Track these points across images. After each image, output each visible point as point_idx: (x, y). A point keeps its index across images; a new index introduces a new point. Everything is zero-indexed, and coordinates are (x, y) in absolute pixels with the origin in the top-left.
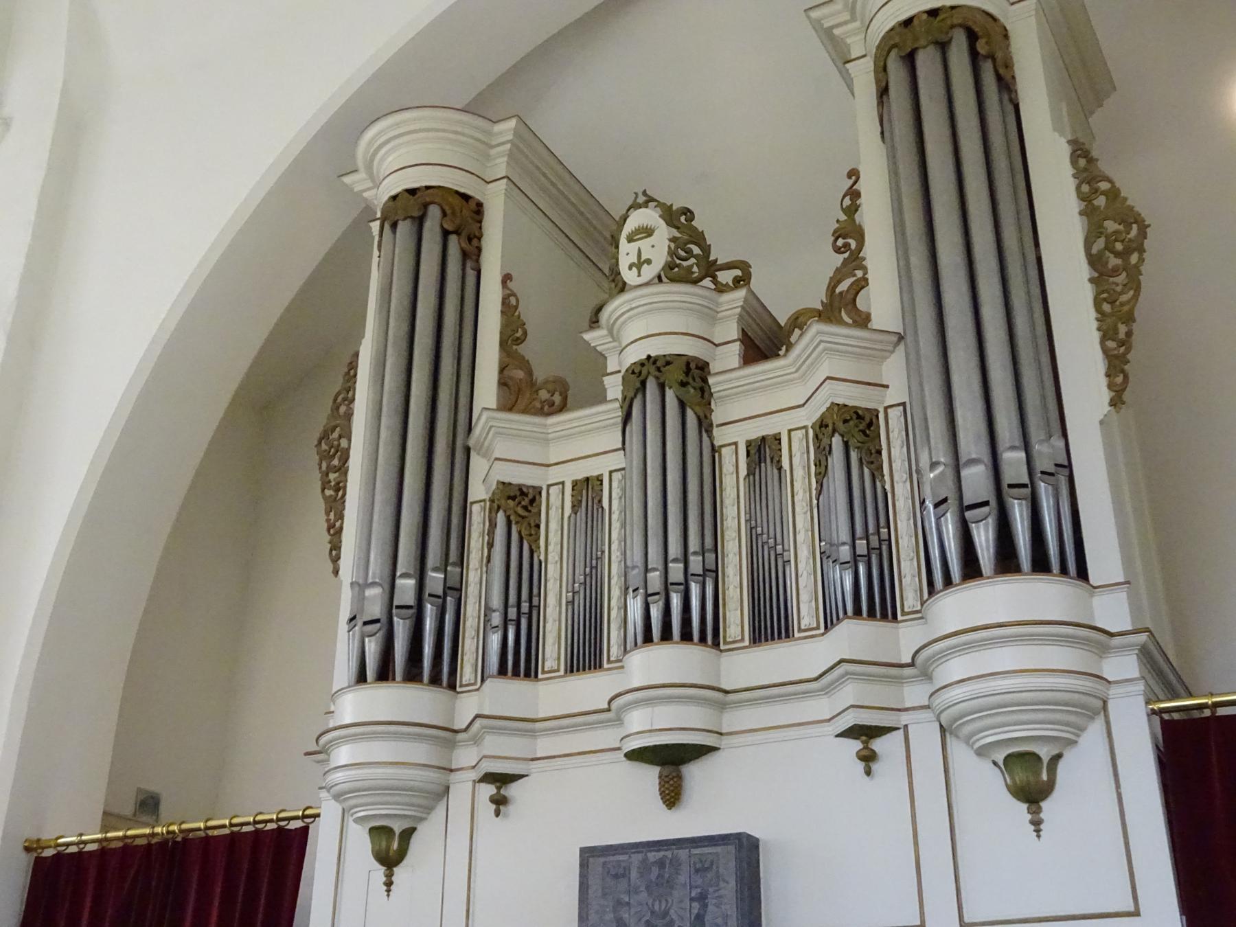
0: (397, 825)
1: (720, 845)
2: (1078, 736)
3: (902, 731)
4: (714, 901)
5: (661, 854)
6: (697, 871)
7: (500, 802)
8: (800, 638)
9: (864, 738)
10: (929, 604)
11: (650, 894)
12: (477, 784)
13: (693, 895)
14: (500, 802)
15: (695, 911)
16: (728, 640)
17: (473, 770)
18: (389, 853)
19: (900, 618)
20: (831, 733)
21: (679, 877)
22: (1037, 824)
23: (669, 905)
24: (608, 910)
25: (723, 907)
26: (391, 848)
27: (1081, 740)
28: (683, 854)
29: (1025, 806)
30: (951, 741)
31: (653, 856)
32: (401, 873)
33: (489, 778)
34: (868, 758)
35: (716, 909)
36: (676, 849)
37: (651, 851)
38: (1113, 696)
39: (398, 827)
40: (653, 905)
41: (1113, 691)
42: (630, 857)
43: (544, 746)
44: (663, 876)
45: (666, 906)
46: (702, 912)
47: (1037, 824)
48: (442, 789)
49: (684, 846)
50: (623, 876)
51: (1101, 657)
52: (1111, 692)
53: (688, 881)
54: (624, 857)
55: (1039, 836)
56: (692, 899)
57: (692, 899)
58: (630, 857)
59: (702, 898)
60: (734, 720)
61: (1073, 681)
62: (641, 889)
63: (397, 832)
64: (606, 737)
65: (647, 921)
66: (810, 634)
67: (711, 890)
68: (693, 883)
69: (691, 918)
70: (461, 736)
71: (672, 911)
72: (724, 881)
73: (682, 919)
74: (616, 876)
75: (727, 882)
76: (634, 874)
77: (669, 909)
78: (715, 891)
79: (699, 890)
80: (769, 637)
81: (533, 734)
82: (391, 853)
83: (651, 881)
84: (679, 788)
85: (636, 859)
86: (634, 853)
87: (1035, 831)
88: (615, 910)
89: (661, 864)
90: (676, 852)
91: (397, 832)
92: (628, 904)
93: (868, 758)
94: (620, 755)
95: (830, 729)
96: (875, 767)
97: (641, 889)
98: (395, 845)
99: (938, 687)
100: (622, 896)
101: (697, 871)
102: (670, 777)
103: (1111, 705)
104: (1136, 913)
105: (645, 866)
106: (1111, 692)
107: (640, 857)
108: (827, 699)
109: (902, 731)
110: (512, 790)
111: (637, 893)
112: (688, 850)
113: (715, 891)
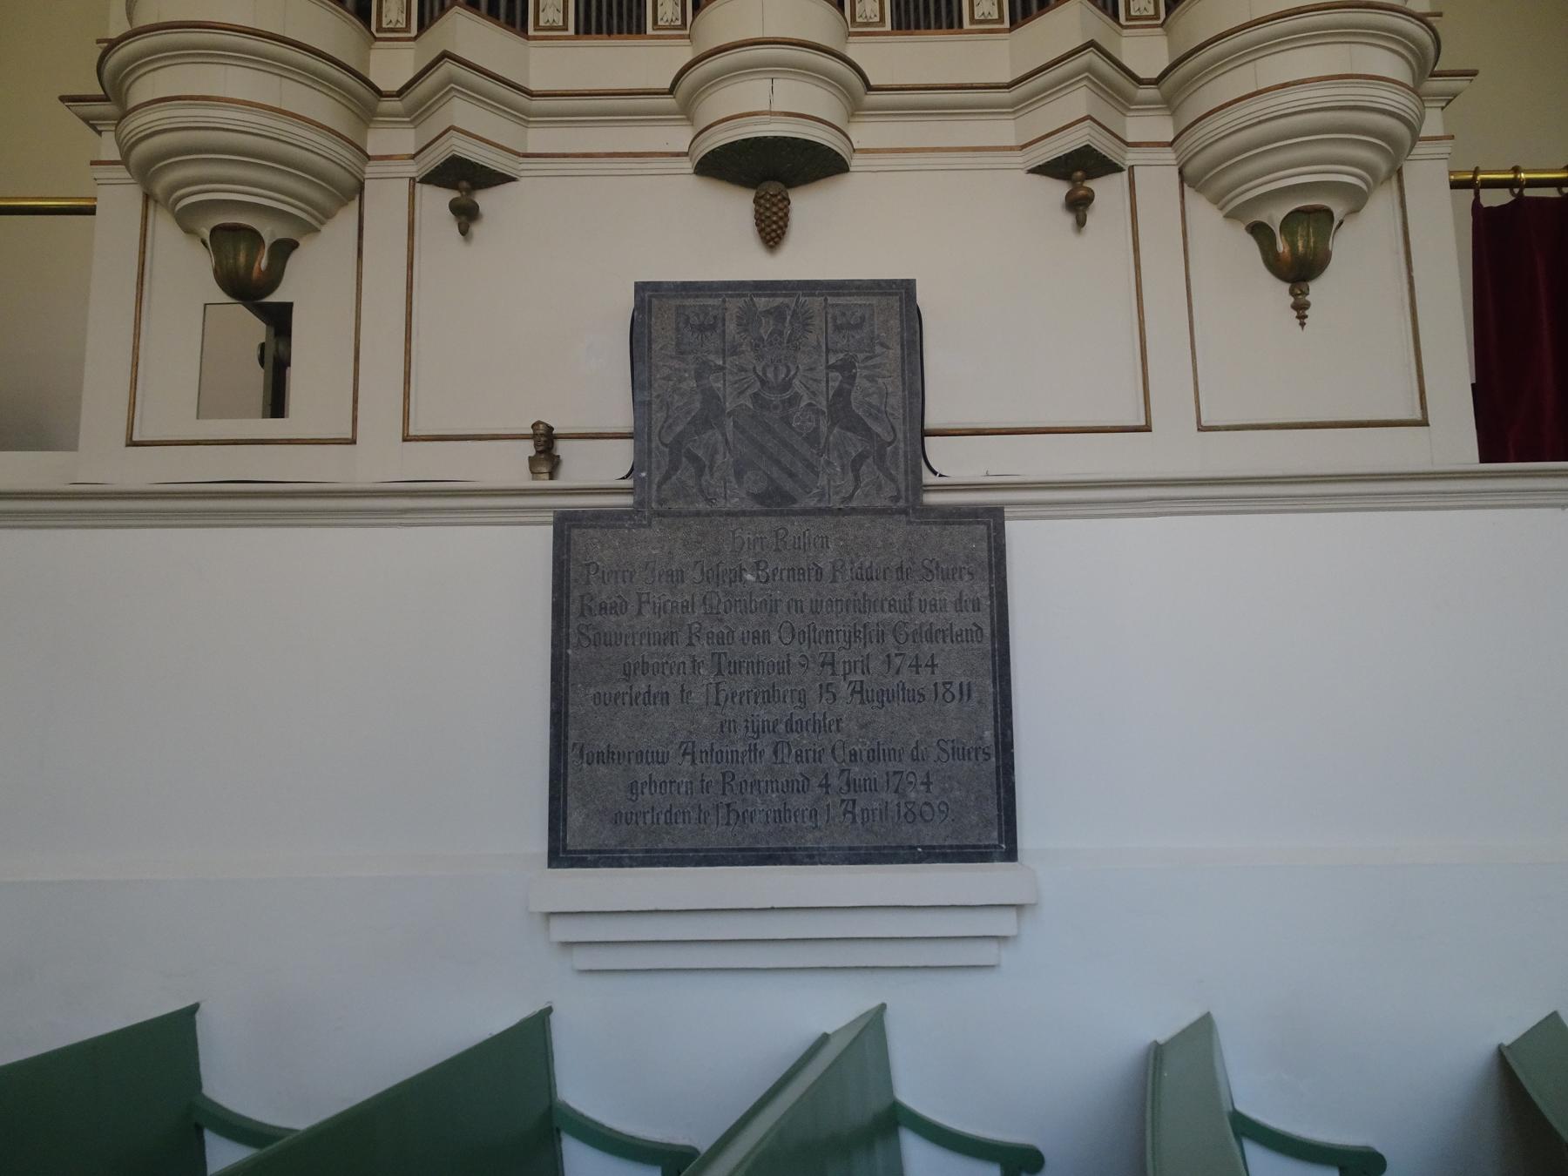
0: (269, 228)
1: (874, 295)
2: (322, 223)
3: (1125, 174)
4: (865, 372)
5: (779, 300)
6: (838, 328)
7: (466, 214)
8: (535, 38)
9: (464, 184)
10: (1177, 14)
11: (760, 357)
12: (418, 185)
13: (832, 361)
14: (466, 214)
15: (834, 384)
16: (996, 16)
17: (1170, 149)
18: (251, 273)
19: (531, 32)
20: (1021, 166)
21: (809, 335)
22: (1301, 309)
23: (792, 373)
24: (687, 375)
25: (880, 380)
26: (257, 265)
27: (325, 230)
28: (815, 303)
29: (1287, 286)
30: (155, 216)
31: (762, 303)
32: (1317, 290)
33: (438, 177)
34: (1078, 205)
35: (868, 384)
36: (804, 295)
37: (760, 296)
38: (371, 176)
39: (270, 232)
40: (765, 374)
41: (371, 169)
42: (724, 301)
43: (538, 139)
44: (781, 334)
45: (787, 376)
46: (846, 386)
47: (1301, 309)
48: (350, 182)
49: (817, 292)
50: (713, 327)
51: (1125, 115)
52: (368, 170)
53: (823, 341)
54: (716, 302)
55: (1302, 325)
56: (829, 368)
57: (829, 368)
58: (724, 301)
59: (846, 367)
60: (865, 133)
61: (339, 148)
62: (744, 348)
63: (268, 242)
64: (1004, 131)
65: (756, 395)
66: (986, 27)
67: (861, 356)
68: (830, 345)
69: (828, 394)
70: (387, 105)
71: (796, 382)
72: (882, 345)
73: (813, 393)
74: (702, 328)
75: (888, 348)
76: (731, 327)
77: (791, 380)
78: (867, 358)
79: (841, 356)
80: (634, 29)
81: (525, 118)
82: (255, 273)
83: (761, 339)
84: (785, 219)
85: (734, 305)
86: (731, 296)
87: (1298, 317)
88: (699, 376)
89: (778, 314)
90: (802, 299)
91: (268, 242)
92: (722, 368)
93: (1078, 205)
94: (688, 165)
95: (1020, 160)
96: (476, 229)
97: (744, 348)
98: (264, 263)
99: (702, 128)
100: (711, 357)
101: (838, 328)
102: (779, 197)
103: (1409, 170)
104: (1424, 423)
105: (747, 320)
106: (368, 170)
107: (741, 302)
108: (413, 130)
109: (1125, 174)
110: (485, 199)
111: (734, 353)
112: (823, 298)
113: (867, 358)
